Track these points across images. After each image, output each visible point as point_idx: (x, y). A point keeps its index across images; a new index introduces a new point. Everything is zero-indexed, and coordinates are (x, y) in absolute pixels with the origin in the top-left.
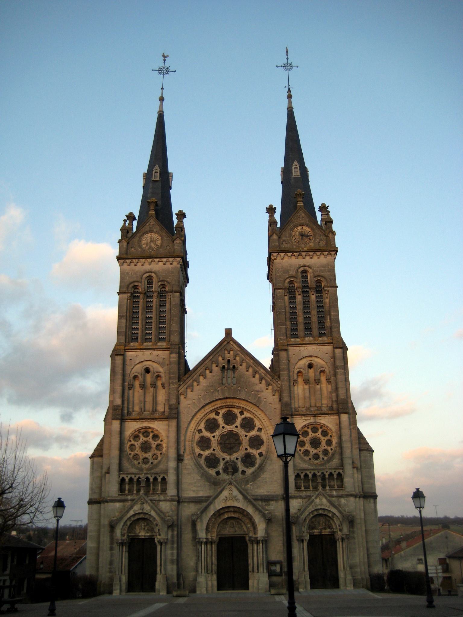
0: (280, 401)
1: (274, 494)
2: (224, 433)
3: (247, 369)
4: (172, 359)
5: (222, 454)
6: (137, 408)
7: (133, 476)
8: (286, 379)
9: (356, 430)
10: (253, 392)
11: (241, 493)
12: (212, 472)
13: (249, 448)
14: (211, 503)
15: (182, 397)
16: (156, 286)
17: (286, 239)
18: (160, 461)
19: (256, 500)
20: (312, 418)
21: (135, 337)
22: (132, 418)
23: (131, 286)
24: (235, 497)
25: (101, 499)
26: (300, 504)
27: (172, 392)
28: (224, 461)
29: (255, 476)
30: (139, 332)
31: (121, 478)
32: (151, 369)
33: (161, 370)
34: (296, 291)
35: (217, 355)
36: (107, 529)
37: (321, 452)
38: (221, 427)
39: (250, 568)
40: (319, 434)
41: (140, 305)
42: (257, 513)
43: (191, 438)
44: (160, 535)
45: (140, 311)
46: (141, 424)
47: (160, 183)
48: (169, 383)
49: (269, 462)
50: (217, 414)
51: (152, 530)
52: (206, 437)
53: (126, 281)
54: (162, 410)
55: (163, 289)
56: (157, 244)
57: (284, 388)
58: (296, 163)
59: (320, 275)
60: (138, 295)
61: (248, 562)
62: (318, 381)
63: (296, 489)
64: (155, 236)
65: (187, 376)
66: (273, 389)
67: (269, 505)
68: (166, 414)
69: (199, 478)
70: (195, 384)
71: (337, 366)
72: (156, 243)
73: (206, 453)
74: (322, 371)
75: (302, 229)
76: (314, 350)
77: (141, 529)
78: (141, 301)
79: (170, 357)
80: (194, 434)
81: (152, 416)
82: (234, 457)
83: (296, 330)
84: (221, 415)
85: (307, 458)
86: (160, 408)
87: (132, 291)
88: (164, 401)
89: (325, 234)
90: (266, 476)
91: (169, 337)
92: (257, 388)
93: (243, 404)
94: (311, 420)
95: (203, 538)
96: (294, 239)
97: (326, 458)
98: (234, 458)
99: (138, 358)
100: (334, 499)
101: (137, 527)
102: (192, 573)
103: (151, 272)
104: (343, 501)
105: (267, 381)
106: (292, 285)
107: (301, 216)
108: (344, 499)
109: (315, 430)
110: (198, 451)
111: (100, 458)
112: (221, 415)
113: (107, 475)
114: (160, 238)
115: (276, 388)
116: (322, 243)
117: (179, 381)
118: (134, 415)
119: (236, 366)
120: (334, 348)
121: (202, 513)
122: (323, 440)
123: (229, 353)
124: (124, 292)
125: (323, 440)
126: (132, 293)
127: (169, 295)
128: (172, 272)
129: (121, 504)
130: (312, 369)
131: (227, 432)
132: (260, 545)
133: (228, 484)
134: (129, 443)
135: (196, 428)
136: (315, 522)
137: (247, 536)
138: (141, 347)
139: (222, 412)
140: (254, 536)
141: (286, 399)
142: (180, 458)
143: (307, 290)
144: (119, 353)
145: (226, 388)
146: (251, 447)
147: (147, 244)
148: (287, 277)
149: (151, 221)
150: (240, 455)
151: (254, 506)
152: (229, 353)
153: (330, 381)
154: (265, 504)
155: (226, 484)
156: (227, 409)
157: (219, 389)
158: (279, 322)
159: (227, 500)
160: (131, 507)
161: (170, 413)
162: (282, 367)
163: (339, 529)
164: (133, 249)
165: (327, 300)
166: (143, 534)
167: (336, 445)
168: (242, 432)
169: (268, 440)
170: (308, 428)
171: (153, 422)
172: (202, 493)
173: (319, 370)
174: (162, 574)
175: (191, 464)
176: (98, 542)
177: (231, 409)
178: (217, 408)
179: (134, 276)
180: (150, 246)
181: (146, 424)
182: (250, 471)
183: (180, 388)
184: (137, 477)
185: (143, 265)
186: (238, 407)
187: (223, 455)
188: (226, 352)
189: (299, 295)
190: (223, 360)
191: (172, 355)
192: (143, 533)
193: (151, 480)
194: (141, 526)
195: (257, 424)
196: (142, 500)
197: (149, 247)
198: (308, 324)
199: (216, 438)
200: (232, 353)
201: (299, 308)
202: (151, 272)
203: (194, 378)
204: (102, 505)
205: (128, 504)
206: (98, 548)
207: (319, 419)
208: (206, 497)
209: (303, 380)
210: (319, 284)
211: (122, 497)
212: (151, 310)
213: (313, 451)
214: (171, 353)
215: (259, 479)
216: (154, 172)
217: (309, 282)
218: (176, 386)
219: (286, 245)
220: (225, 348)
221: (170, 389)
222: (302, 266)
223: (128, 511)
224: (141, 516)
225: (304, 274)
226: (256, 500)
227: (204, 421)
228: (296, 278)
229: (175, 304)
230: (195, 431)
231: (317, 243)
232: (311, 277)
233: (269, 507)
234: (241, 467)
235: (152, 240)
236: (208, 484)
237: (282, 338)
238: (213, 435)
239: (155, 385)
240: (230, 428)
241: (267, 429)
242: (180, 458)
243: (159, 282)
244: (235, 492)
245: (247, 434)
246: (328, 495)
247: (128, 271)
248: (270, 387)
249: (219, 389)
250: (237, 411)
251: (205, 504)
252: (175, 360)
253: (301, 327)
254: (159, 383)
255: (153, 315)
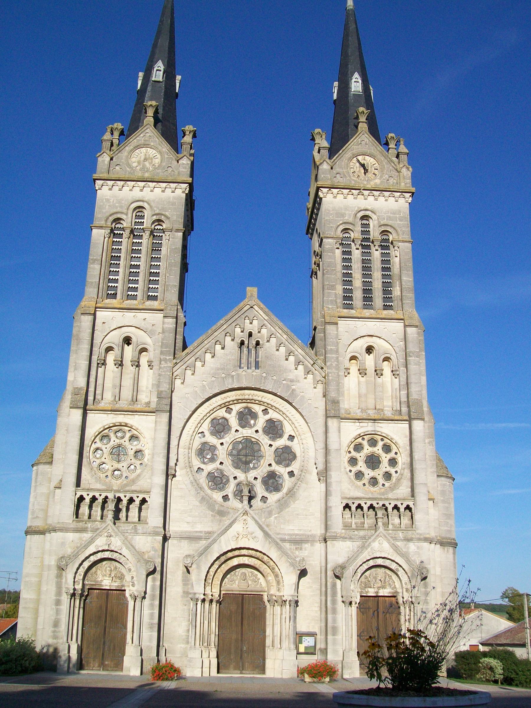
0: (324, 396)
1: (310, 533)
2: (238, 440)
3: (278, 348)
4: (166, 326)
5: (233, 470)
6: (108, 396)
7: (97, 495)
8: (334, 365)
9: (433, 446)
10: (284, 382)
11: (261, 527)
12: (217, 496)
13: (274, 464)
14: (215, 541)
15: (178, 382)
16: (149, 221)
17: (341, 170)
18: (139, 475)
19: (283, 540)
20: (370, 424)
21: (113, 292)
22: (101, 408)
23: (111, 219)
24: (252, 534)
25: (46, 527)
26: (348, 549)
27: (163, 373)
28: (236, 481)
29: (282, 504)
30: (119, 285)
31: (78, 496)
32: (134, 340)
33: (148, 340)
34: (353, 244)
35: (234, 324)
36: (54, 571)
37: (381, 476)
38: (233, 430)
39: (268, 642)
40: (378, 450)
41: (123, 247)
42: (284, 559)
43: (187, 444)
44: (133, 585)
45: (123, 255)
46: (113, 418)
47: (164, 83)
48: (161, 360)
49: (303, 485)
50: (229, 410)
51: (121, 577)
52: (211, 444)
53: (104, 211)
54: (147, 400)
55: (159, 227)
56: (153, 163)
57: (330, 378)
58: (356, 75)
59: (389, 224)
60: (121, 232)
61: (265, 632)
62: (378, 373)
63: (344, 526)
64: (151, 152)
65: (186, 351)
66: (314, 379)
67: (301, 549)
68: (153, 406)
69: (198, 504)
70: (199, 364)
71: (410, 352)
72: (152, 162)
73: (210, 467)
74: (387, 359)
75: (365, 160)
76: (375, 327)
77: (106, 575)
78: (124, 240)
79: (164, 323)
80: (193, 437)
81: (131, 408)
82: (251, 475)
83: (350, 298)
84: (234, 413)
85: (360, 483)
86: (143, 398)
87: (113, 226)
88: (150, 386)
89: (397, 170)
90: (296, 506)
91: (162, 295)
92: (291, 376)
93: (268, 398)
94: (368, 427)
95: (200, 594)
96: (353, 173)
97: (387, 484)
98: (252, 477)
99: (115, 322)
100: (399, 544)
101: (99, 572)
102: (179, 646)
103: (143, 201)
104: (412, 547)
105: (306, 367)
106: (347, 235)
107: (363, 143)
108: (414, 545)
109: (373, 443)
110: (196, 463)
111: (47, 466)
112: (234, 413)
113: (57, 491)
114: (159, 156)
115: (319, 378)
116: (391, 181)
117: (174, 358)
118: (102, 405)
119: (261, 342)
120: (405, 326)
121: (201, 555)
122: (383, 458)
123: (251, 323)
124: (101, 225)
125: (385, 458)
126: (112, 228)
127: (167, 235)
128: (173, 204)
129: (77, 535)
130: (371, 355)
131: (242, 438)
132: (286, 608)
133: (242, 514)
134: (94, 446)
135: (197, 429)
136: (370, 577)
137: (266, 593)
138: (121, 306)
139: (236, 408)
140: (278, 594)
141: (333, 394)
142: (169, 474)
143: (368, 244)
144: (88, 312)
145: (244, 373)
146: (278, 463)
147: (139, 162)
148: (341, 222)
149: (147, 131)
150: (261, 474)
151: (279, 548)
152: (251, 323)
153: (398, 373)
154: (295, 547)
155: (237, 514)
156: (244, 405)
157: (234, 373)
158: (328, 285)
159: (240, 538)
160: (92, 541)
161: (158, 403)
162: (329, 347)
163: (406, 589)
164: (118, 168)
165: (397, 260)
166: (107, 583)
167: (404, 466)
168: (264, 440)
169: (303, 454)
170: (363, 439)
171: (132, 416)
172: (201, 527)
173: (383, 357)
174: (134, 645)
175: (186, 482)
176: (39, 592)
177: (250, 405)
178: (229, 402)
179: (117, 205)
180: (144, 166)
181: (120, 418)
182: (273, 497)
183: (175, 369)
184: (103, 496)
185: (131, 190)
186: (260, 403)
187: (235, 472)
188: (247, 321)
189: (357, 249)
190: (242, 332)
191: (166, 320)
192: (108, 581)
193: (125, 502)
194: (105, 571)
195: (288, 430)
196: (109, 531)
197: (142, 166)
198: (367, 292)
199: (225, 446)
200: (255, 322)
201: (356, 267)
202: (143, 201)
203: (197, 355)
204: (47, 535)
205: (87, 536)
206: (38, 601)
207: (381, 427)
208: (206, 533)
209: (359, 370)
210: (385, 237)
211: (80, 525)
212: (139, 256)
213: (369, 473)
214: (165, 317)
215: (287, 510)
216: (155, 70)
217: (371, 233)
218: (170, 365)
219: (342, 179)
220: (246, 314)
221: (160, 368)
222: (363, 210)
223: (86, 546)
224: (107, 555)
225: (365, 222)
226: (283, 540)
227: (209, 420)
228: (354, 225)
229: (176, 248)
230: (195, 433)
231: (385, 181)
232: (374, 226)
233: (301, 551)
234: (260, 490)
235: (147, 156)
236: (211, 513)
237: (330, 307)
238: (221, 441)
239: (138, 362)
240: (247, 432)
241: (303, 437)
242: (169, 474)
243: (153, 215)
244: (252, 526)
245: (272, 443)
246: (392, 537)
247: (108, 197)
248: (310, 376)
249: (234, 373)
250: (257, 409)
251: (203, 543)
252: (171, 326)
253: (358, 295)
254: (144, 359)
255: (142, 263)
